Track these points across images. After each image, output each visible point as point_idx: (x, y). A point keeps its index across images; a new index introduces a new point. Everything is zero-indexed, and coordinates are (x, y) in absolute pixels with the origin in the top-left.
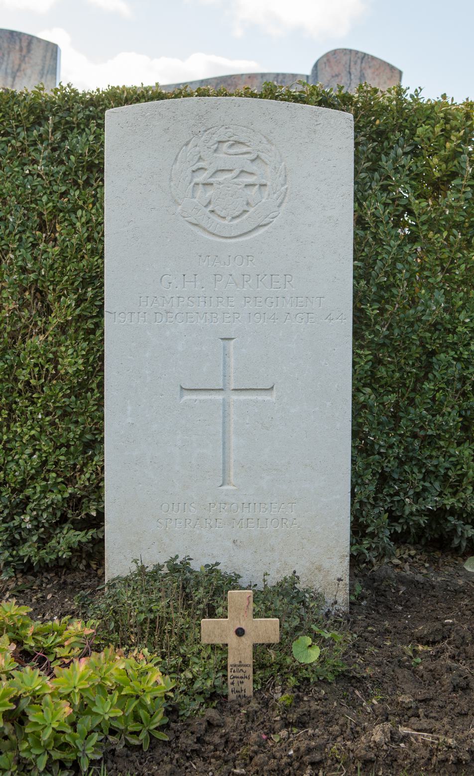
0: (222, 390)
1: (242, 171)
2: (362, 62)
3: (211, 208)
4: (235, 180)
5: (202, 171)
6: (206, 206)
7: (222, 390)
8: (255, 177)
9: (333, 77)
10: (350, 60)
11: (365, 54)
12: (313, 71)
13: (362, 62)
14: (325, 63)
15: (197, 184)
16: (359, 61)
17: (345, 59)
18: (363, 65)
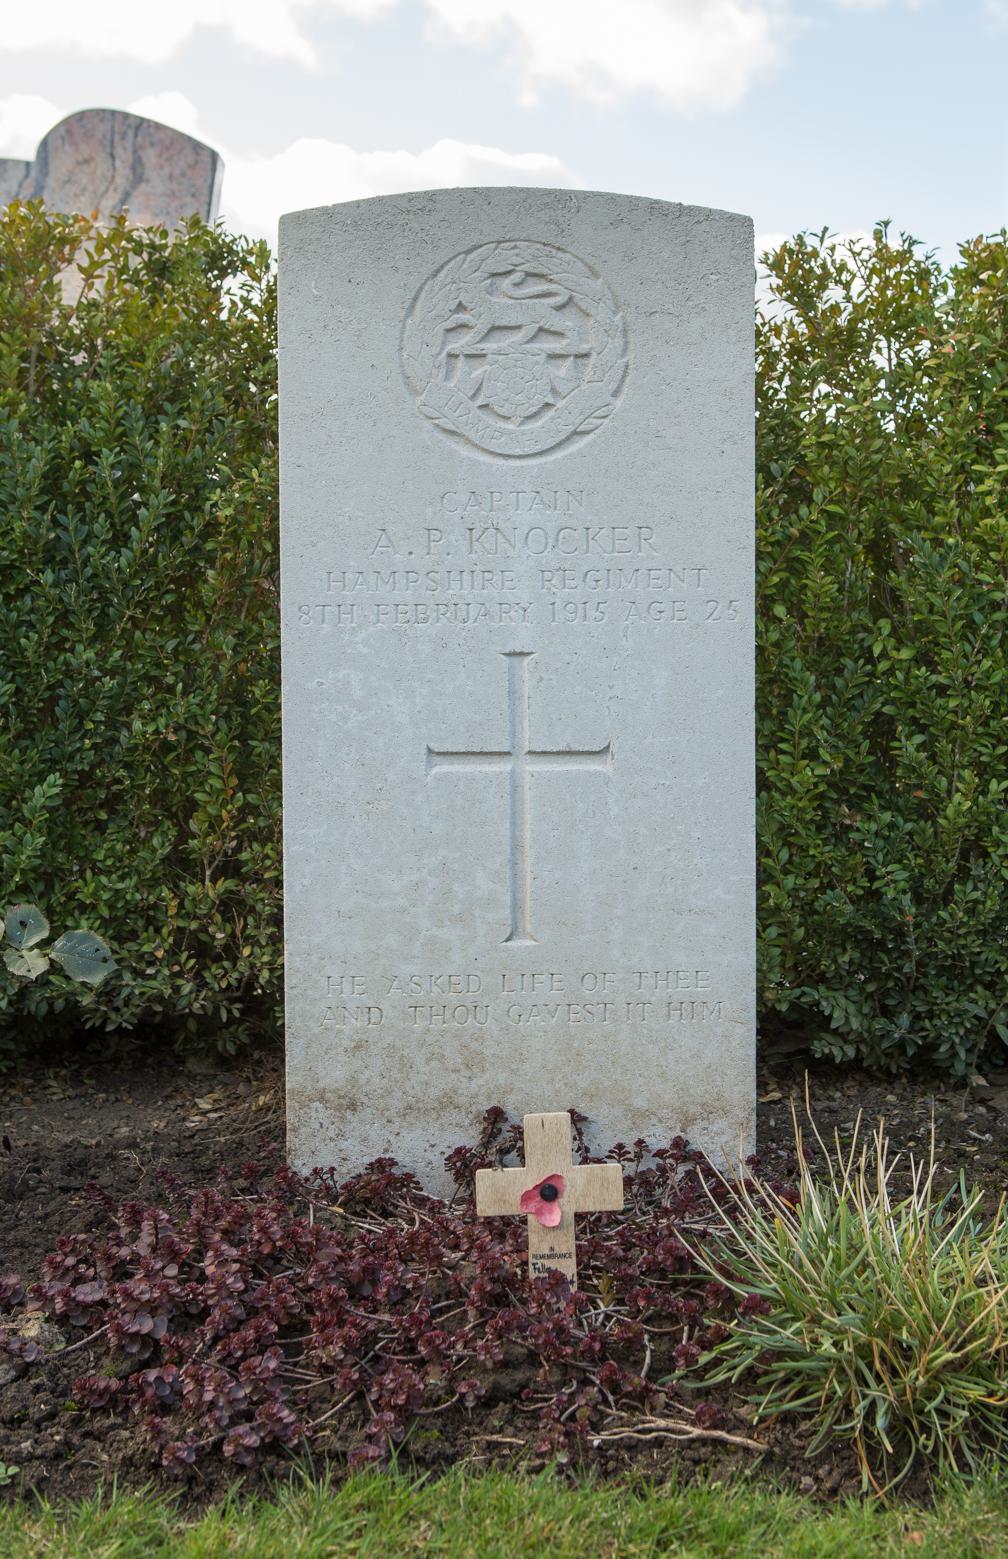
0: (508, 753)
1: (541, 329)
2: (136, 136)
3: (480, 401)
4: (528, 346)
5: (465, 330)
6: (474, 397)
7: (508, 753)
8: (565, 342)
9: (78, 164)
10: (113, 131)
11: (142, 120)
12: (39, 152)
13: (136, 136)
14: (63, 138)
15: (452, 356)
16: (131, 134)
17: (102, 129)
18: (140, 139)
